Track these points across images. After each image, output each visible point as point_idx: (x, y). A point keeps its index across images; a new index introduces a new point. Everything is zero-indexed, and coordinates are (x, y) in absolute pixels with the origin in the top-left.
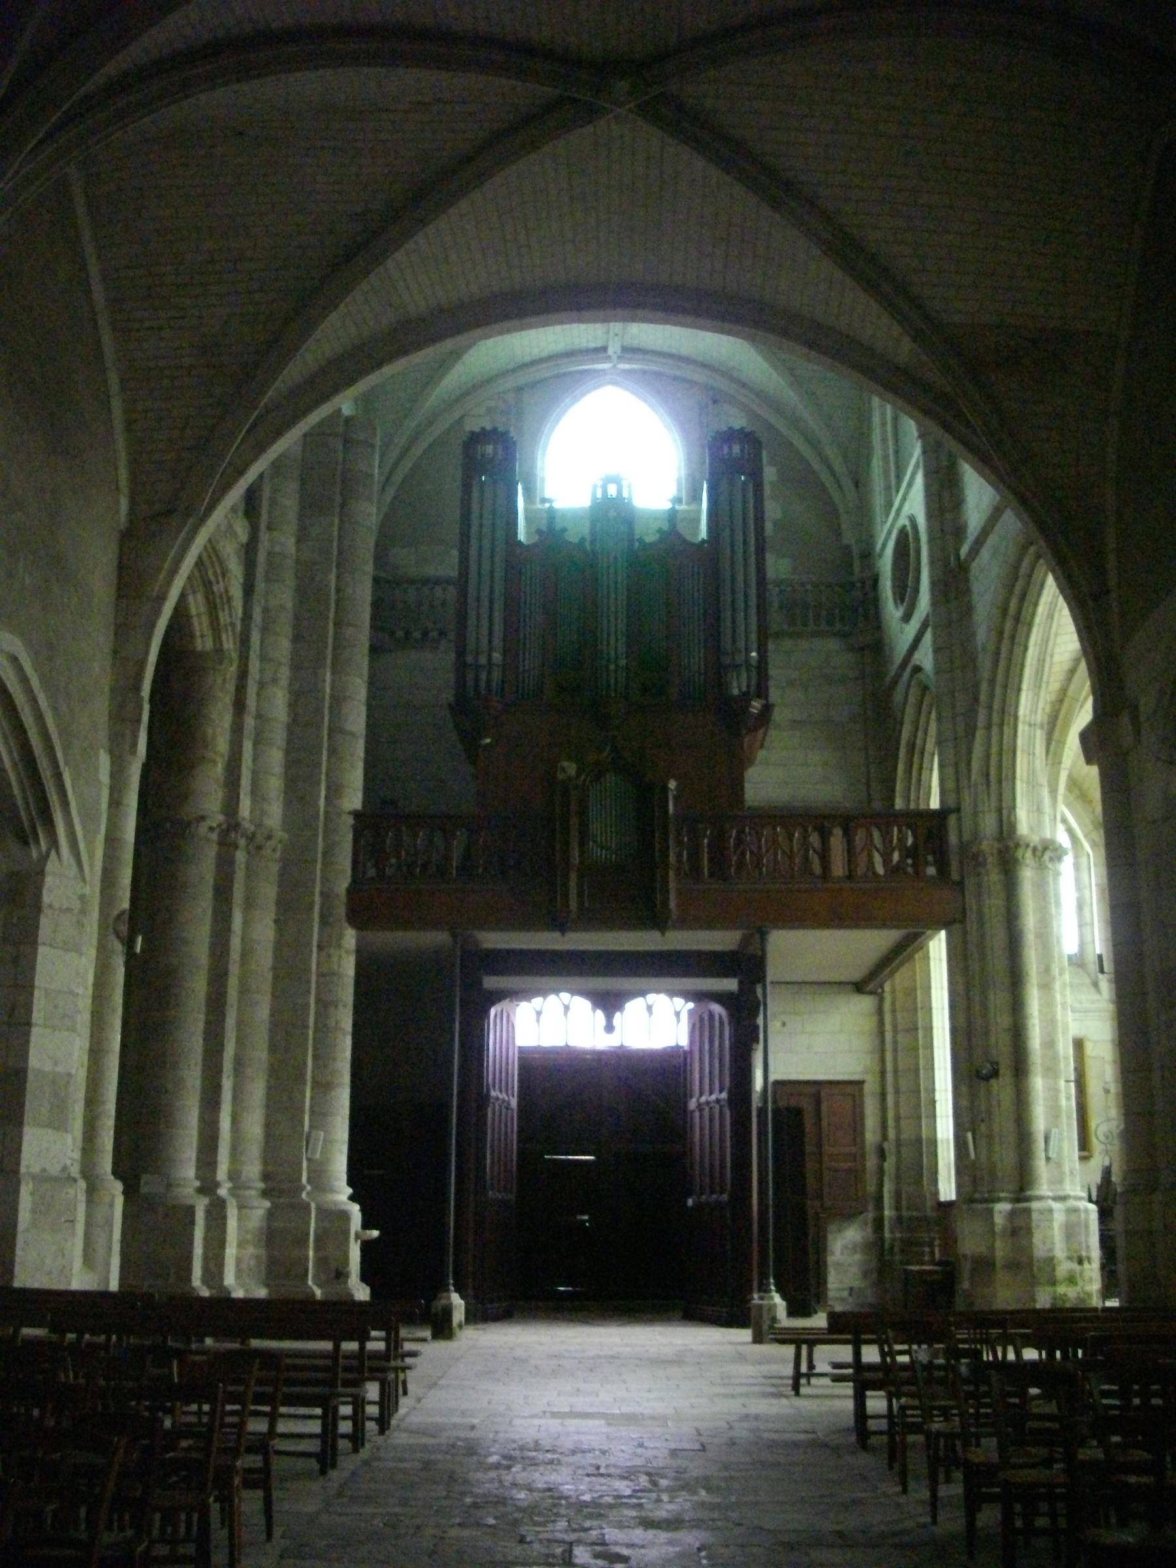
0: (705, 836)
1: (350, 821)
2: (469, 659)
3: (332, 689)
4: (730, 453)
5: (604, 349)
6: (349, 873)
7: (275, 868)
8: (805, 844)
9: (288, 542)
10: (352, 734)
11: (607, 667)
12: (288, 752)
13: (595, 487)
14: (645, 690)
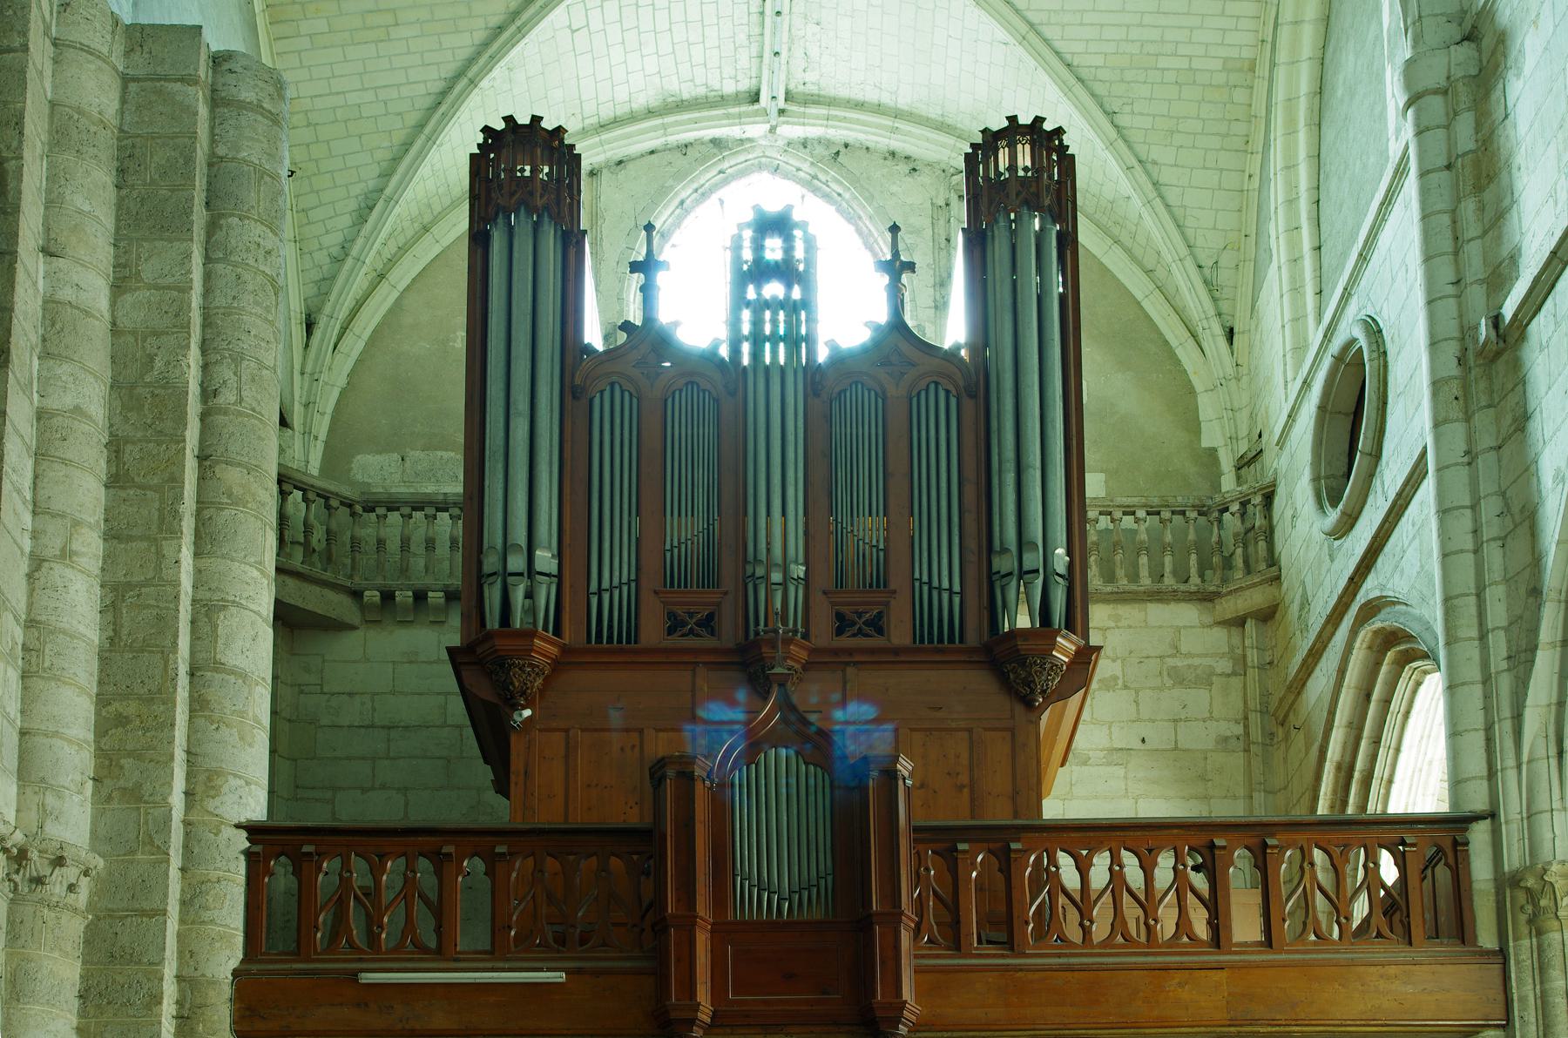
0: (973, 866)
1: (241, 841)
2: (491, 563)
3: (195, 587)
4: (1012, 167)
5: (755, 97)
6: (239, 939)
7: (74, 927)
8: (1180, 884)
9: (94, 289)
10: (244, 676)
11: (767, 577)
12: (102, 701)
13: (737, 247)
14: (842, 624)
